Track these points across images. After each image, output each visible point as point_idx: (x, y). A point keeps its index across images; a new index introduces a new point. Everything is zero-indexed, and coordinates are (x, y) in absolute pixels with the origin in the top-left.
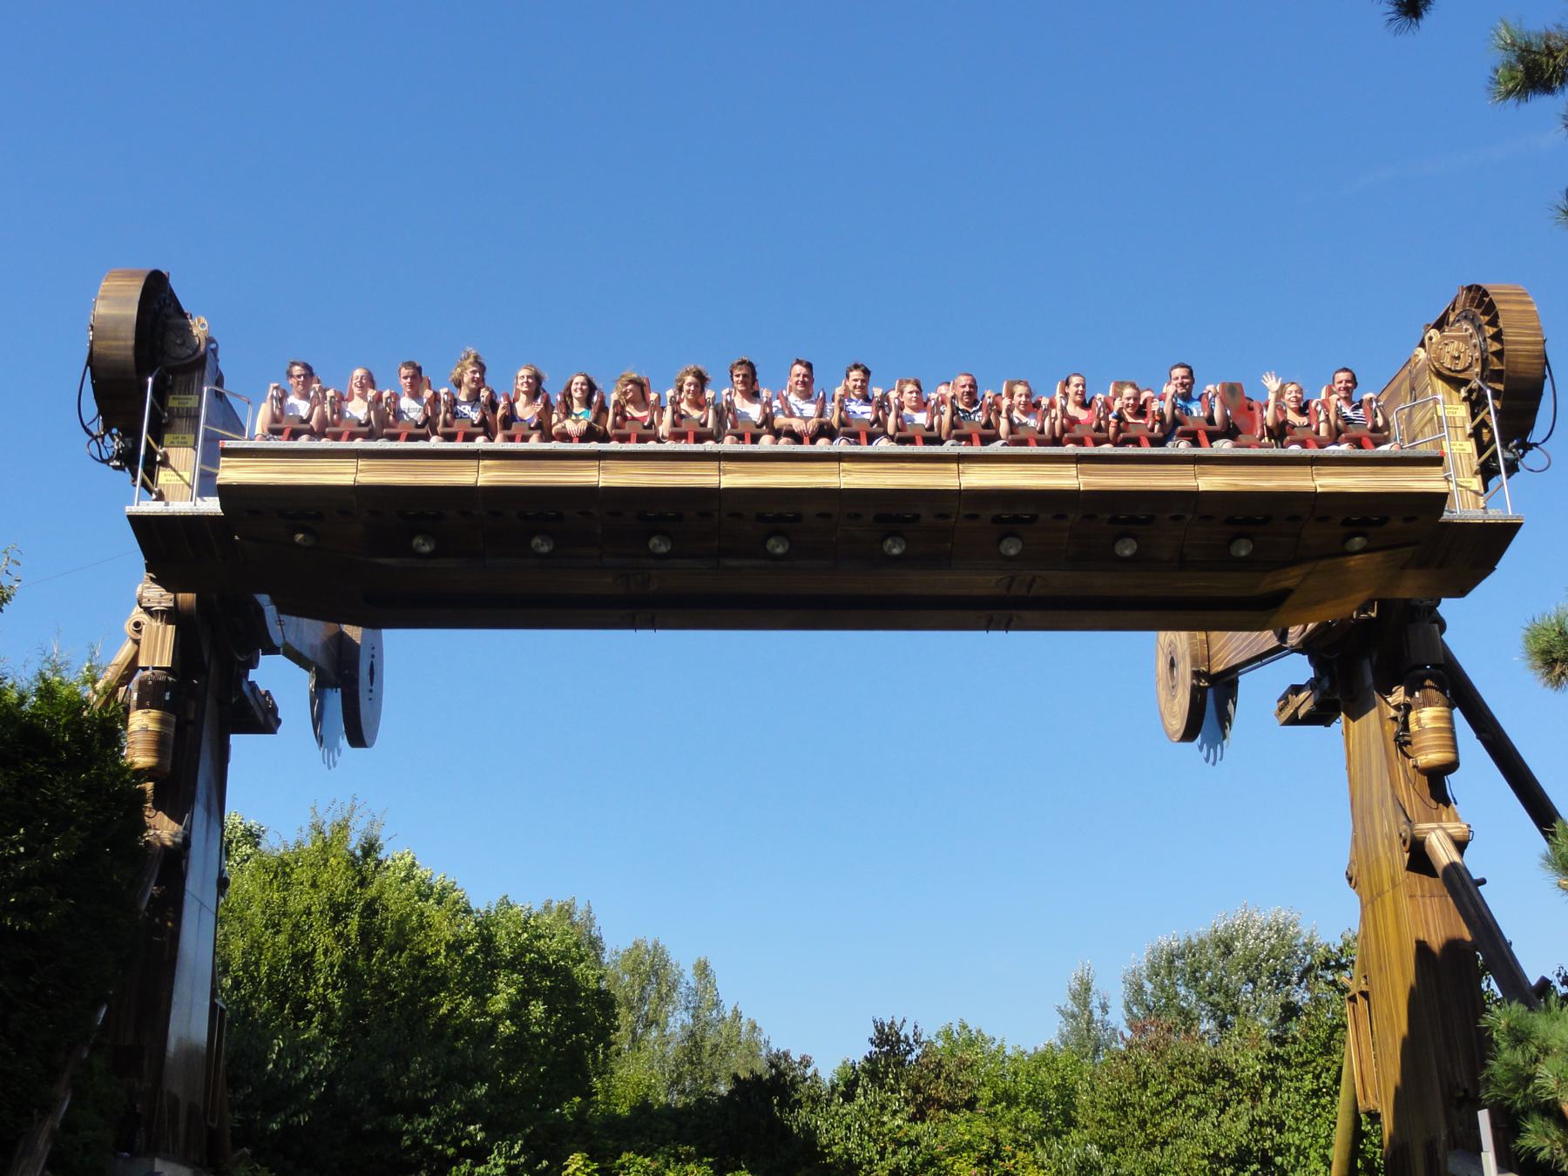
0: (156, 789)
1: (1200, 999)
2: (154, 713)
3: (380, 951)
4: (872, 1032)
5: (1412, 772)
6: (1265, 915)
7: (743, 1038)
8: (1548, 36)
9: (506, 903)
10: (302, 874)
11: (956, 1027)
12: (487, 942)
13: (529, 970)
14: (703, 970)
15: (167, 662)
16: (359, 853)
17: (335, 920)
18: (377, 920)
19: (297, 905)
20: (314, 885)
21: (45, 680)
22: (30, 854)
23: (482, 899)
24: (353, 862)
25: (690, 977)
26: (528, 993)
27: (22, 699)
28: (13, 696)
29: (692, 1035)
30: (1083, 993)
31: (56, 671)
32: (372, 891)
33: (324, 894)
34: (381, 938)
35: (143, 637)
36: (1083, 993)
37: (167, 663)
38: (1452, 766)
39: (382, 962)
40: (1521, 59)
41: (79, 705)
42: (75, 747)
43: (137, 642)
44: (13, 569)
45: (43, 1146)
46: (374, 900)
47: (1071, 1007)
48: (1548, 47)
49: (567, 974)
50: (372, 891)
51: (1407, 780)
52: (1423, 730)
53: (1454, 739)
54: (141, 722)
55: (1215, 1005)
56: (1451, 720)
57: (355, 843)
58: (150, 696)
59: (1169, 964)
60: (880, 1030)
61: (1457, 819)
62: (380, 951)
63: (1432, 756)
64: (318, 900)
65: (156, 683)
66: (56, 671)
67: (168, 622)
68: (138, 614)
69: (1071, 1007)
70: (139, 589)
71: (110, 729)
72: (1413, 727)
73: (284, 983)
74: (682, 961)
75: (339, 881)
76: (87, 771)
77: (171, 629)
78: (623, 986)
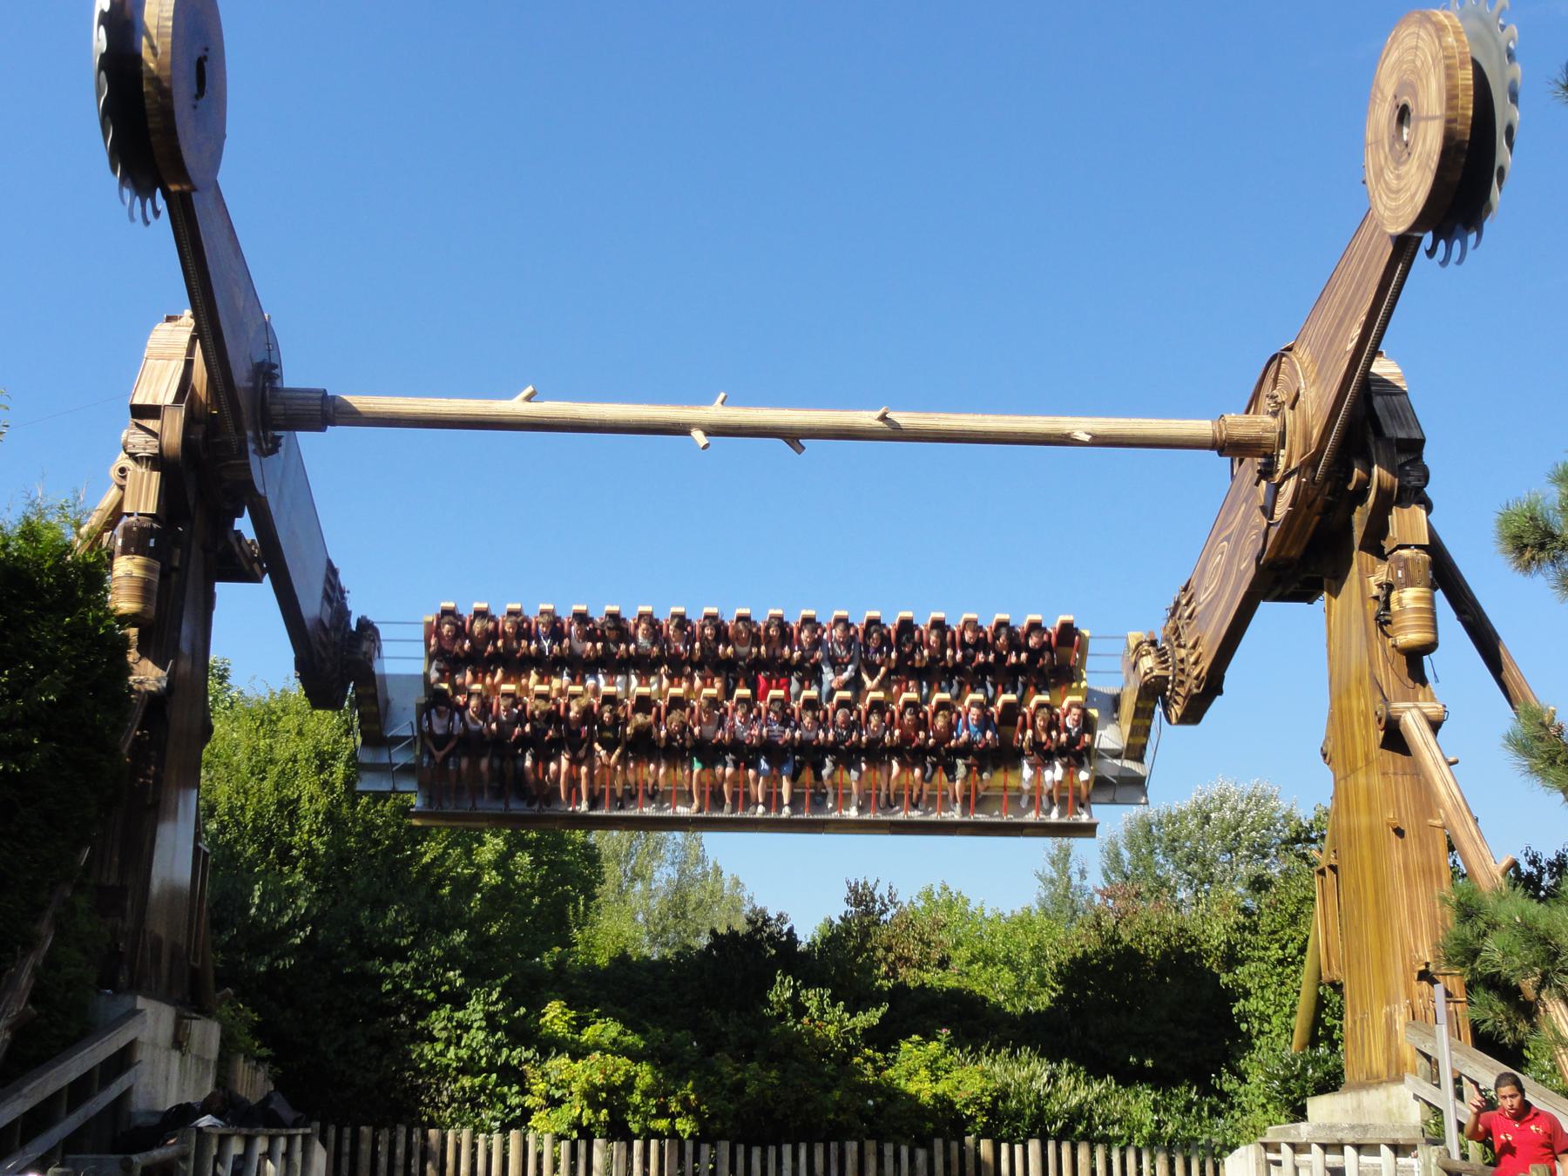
0: (141, 636)
1: (1177, 867)
2: (139, 559)
4: (845, 892)
11: (937, 889)
15: (152, 509)
17: (321, 769)
20: (300, 733)
29: (678, 889)
33: (310, 742)
35: (128, 483)
37: (152, 510)
38: (1430, 647)
43: (122, 488)
45: (25, 980)
51: (1386, 659)
52: (1403, 610)
53: (1434, 620)
54: (126, 569)
56: (1432, 601)
58: (136, 543)
60: (854, 890)
61: (1433, 700)
63: (1411, 637)
64: (304, 748)
65: (141, 529)
67: (154, 469)
68: (123, 460)
70: (124, 435)
71: (94, 575)
72: (1394, 607)
73: (269, 828)
77: (156, 475)
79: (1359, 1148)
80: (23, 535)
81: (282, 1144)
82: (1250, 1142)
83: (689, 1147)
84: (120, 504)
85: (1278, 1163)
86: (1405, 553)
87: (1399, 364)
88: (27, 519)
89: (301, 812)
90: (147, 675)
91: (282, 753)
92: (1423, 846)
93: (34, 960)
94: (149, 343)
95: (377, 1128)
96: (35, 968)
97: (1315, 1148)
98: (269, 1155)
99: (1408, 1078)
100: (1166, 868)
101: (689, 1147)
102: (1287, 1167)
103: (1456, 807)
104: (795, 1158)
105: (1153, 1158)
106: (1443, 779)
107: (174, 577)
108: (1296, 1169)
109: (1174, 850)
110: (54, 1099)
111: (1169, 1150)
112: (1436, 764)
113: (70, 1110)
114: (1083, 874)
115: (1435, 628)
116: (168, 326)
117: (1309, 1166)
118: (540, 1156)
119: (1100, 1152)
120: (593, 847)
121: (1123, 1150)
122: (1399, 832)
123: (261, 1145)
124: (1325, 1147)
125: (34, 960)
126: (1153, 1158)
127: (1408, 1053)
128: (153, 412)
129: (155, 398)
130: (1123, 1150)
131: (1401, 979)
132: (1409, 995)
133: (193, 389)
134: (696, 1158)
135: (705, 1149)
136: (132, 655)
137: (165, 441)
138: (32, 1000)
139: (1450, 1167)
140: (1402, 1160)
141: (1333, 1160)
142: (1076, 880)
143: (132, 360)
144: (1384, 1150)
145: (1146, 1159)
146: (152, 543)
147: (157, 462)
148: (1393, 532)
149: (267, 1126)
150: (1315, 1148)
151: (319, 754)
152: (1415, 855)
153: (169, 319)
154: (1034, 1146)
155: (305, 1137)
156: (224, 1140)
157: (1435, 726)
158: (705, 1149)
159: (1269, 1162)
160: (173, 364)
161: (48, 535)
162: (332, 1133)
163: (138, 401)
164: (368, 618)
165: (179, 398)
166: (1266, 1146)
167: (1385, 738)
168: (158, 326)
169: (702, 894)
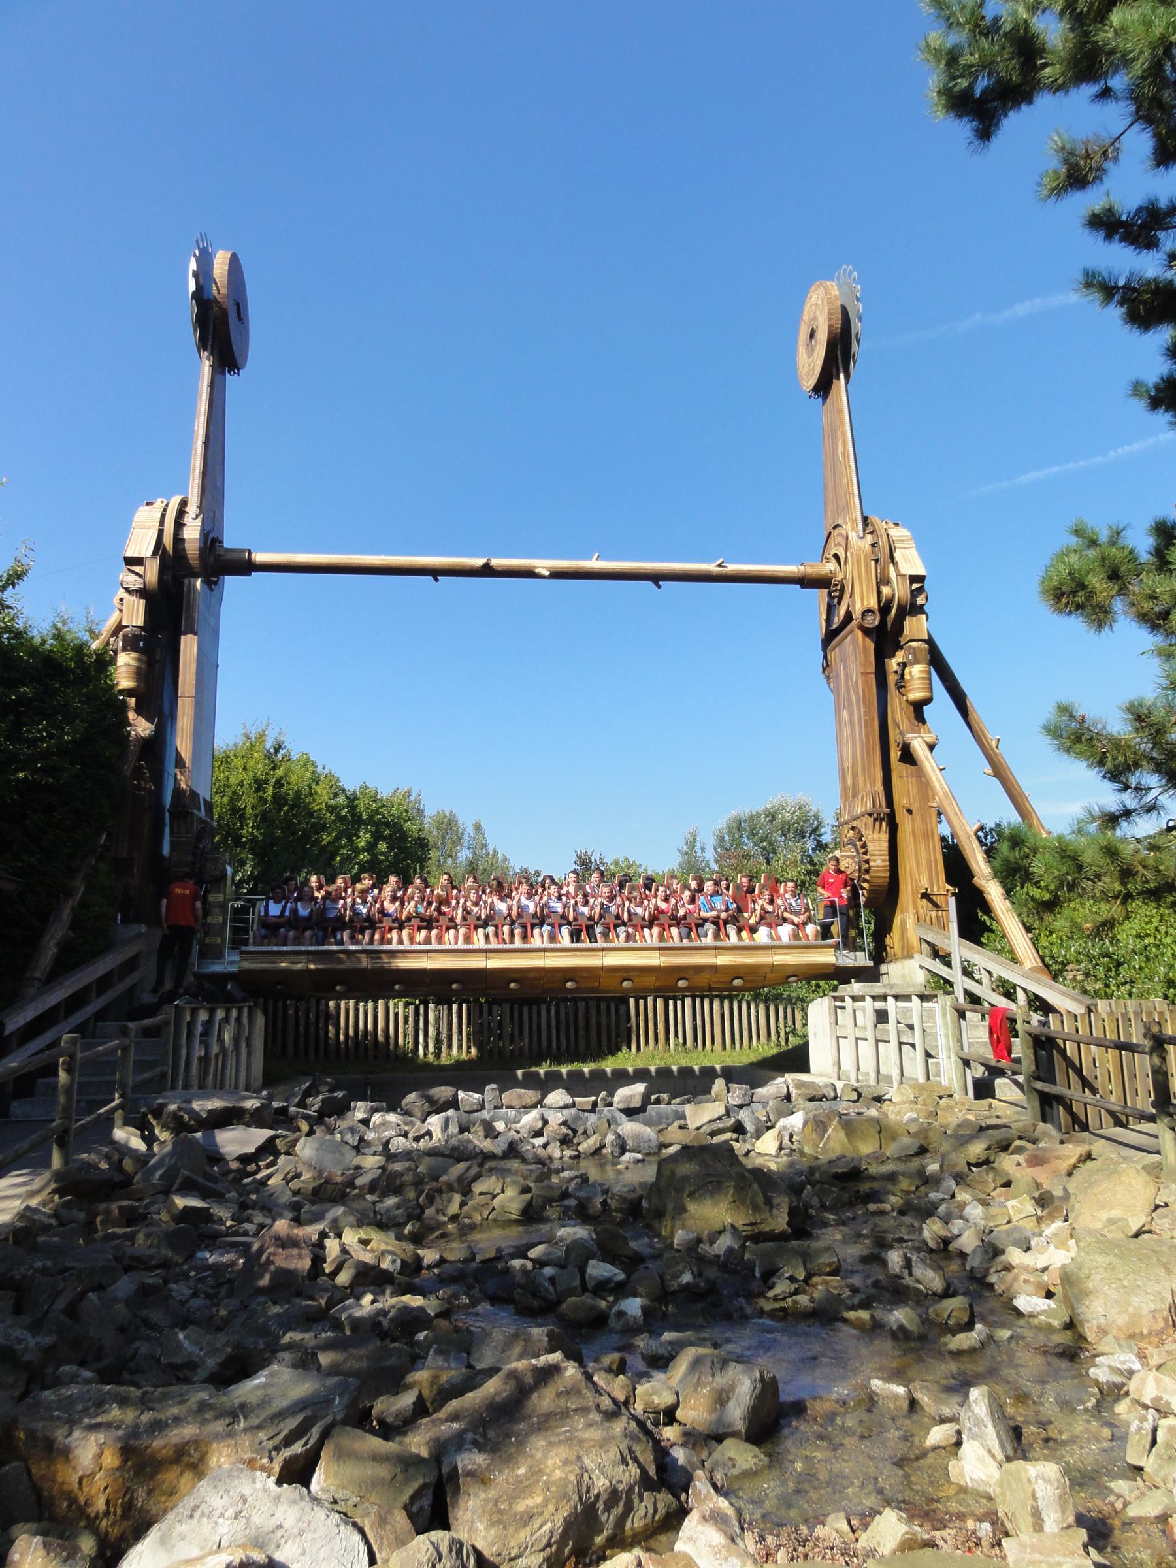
0: (137, 703)
1: (755, 845)
2: (133, 654)
3: (286, 808)
4: (574, 858)
5: (904, 704)
6: (791, 800)
7: (500, 864)
8: (1086, 143)
9: (364, 787)
10: (238, 762)
11: (622, 860)
12: (352, 808)
13: (378, 824)
14: (478, 827)
15: (140, 622)
16: (272, 751)
17: (258, 790)
18: (283, 790)
19: (234, 781)
20: (245, 769)
21: (57, 629)
22: (50, 736)
23: (351, 784)
24: (269, 756)
25: (470, 831)
26: (377, 837)
27: (43, 642)
28: (37, 640)
29: (471, 863)
30: (692, 841)
31: (64, 623)
32: (280, 772)
33: (251, 774)
34: (286, 800)
35: (124, 608)
36: (692, 841)
37: (141, 623)
38: (928, 701)
39: (286, 813)
40: (1066, 161)
41: (80, 648)
42: (78, 671)
43: (121, 611)
44: (29, 553)
45: (66, 915)
46: (281, 778)
47: (685, 848)
48: (1087, 151)
49: (401, 829)
50: (280, 772)
51: (902, 709)
52: (912, 679)
53: (931, 684)
54: (126, 661)
55: (764, 849)
56: (929, 673)
57: (269, 745)
58: (131, 644)
59: (737, 826)
60: (579, 857)
61: (930, 732)
62: (286, 808)
63: (916, 694)
64: (247, 778)
65: (134, 636)
66: (64, 623)
67: (141, 597)
68: (121, 593)
69: (685, 848)
70: (121, 577)
71: (104, 661)
72: (907, 677)
73: (227, 825)
74: (466, 823)
75: (260, 768)
76: (87, 686)
77: (142, 602)
78: (432, 835)
79: (896, 997)
80: (55, 637)
81: (234, 1013)
82: (825, 995)
83: (486, 1008)
84: (120, 621)
85: (844, 1008)
86: (914, 644)
87: (910, 530)
88: (55, 626)
89: (247, 816)
90: (141, 727)
91: (234, 781)
92: (923, 819)
93: (71, 903)
94: (135, 519)
95: (375, 1002)
96: (72, 909)
97: (868, 998)
98: (226, 1020)
99: (916, 956)
100: (749, 846)
101: (486, 1008)
102: (849, 1010)
103: (946, 795)
104: (549, 1012)
105: (757, 1006)
106: (937, 778)
107: (157, 666)
108: (854, 1011)
109: (753, 835)
110: (86, 989)
111: (766, 1001)
112: (933, 769)
113: (99, 995)
114: (703, 850)
115: (931, 689)
116: (148, 508)
117: (864, 1009)
118: (396, 1015)
119: (726, 1004)
120: (424, 839)
121: (740, 1003)
122: (910, 812)
123: (220, 1014)
124: (874, 998)
125: (71, 903)
126: (757, 1006)
127: (915, 942)
128: (139, 561)
129: (140, 552)
130: (740, 1003)
131: (910, 899)
132: (915, 907)
133: (164, 548)
134: (490, 1013)
135: (495, 1008)
136: (131, 715)
137: (147, 580)
138: (72, 927)
139: (960, 1007)
140: (925, 1004)
141: (879, 1005)
142: (699, 854)
143: (124, 529)
144: (915, 998)
145: (753, 1006)
146: (141, 644)
147: (142, 593)
148: (907, 632)
149: (226, 1002)
150: (868, 998)
151: (256, 781)
152: (919, 826)
153: (148, 504)
154: (688, 1001)
155: (250, 1008)
156: (194, 1012)
157: (931, 747)
158: (495, 1008)
159: (836, 1007)
160: (151, 531)
161: (69, 637)
162: (271, 1005)
163: (129, 554)
164: (295, 748)
165: (155, 553)
166: (835, 998)
167: (901, 756)
168: (141, 508)
169: (486, 866)
